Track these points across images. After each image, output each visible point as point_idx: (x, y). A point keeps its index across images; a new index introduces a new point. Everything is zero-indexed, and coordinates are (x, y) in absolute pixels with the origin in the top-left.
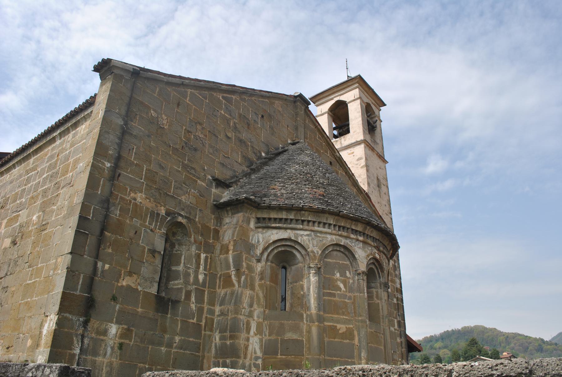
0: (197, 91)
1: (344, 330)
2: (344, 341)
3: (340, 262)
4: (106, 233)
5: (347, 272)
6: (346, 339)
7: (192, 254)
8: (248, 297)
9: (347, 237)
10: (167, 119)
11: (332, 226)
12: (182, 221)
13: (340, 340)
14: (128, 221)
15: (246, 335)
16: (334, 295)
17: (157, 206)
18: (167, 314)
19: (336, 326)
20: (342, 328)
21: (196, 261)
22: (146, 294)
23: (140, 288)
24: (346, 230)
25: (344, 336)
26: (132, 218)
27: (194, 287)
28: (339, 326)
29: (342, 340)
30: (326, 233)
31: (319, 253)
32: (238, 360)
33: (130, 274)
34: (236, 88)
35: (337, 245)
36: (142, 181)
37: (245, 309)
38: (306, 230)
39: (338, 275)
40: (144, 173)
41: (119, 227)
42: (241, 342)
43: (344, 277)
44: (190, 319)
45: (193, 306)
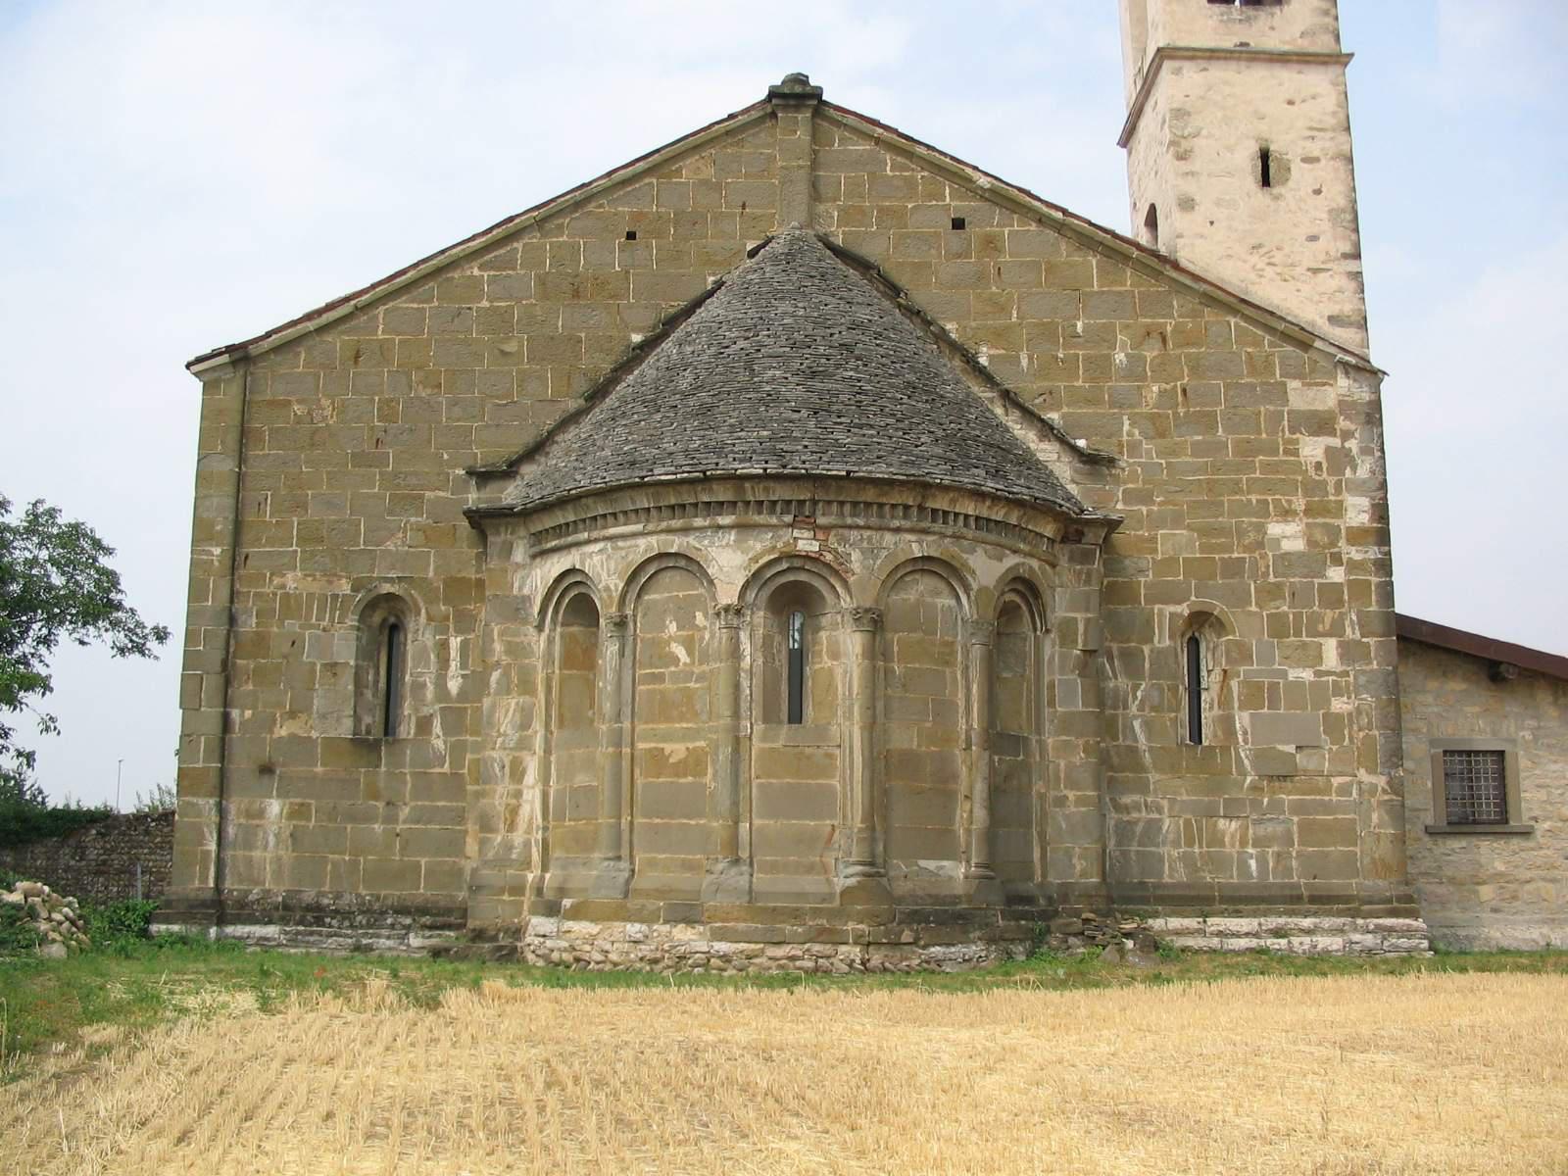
0: (404, 298)
1: (682, 755)
2: (682, 780)
3: (681, 594)
4: (238, 661)
5: (697, 614)
7: (425, 646)
9: (686, 530)
10: (333, 403)
11: (653, 512)
12: (392, 590)
14: (275, 629)
15: (512, 787)
16: (659, 678)
17: (330, 582)
18: (378, 766)
19: (663, 749)
20: (676, 750)
21: (438, 656)
22: (329, 742)
23: (314, 734)
25: (681, 768)
26: (281, 621)
28: (668, 747)
30: (634, 535)
32: (489, 835)
33: (292, 715)
34: (517, 221)
35: (661, 556)
36: (294, 548)
37: (505, 735)
38: (596, 540)
39: (673, 628)
40: (295, 533)
41: (261, 643)
42: (497, 803)
43: (689, 630)
44: (434, 767)
45: (439, 744)
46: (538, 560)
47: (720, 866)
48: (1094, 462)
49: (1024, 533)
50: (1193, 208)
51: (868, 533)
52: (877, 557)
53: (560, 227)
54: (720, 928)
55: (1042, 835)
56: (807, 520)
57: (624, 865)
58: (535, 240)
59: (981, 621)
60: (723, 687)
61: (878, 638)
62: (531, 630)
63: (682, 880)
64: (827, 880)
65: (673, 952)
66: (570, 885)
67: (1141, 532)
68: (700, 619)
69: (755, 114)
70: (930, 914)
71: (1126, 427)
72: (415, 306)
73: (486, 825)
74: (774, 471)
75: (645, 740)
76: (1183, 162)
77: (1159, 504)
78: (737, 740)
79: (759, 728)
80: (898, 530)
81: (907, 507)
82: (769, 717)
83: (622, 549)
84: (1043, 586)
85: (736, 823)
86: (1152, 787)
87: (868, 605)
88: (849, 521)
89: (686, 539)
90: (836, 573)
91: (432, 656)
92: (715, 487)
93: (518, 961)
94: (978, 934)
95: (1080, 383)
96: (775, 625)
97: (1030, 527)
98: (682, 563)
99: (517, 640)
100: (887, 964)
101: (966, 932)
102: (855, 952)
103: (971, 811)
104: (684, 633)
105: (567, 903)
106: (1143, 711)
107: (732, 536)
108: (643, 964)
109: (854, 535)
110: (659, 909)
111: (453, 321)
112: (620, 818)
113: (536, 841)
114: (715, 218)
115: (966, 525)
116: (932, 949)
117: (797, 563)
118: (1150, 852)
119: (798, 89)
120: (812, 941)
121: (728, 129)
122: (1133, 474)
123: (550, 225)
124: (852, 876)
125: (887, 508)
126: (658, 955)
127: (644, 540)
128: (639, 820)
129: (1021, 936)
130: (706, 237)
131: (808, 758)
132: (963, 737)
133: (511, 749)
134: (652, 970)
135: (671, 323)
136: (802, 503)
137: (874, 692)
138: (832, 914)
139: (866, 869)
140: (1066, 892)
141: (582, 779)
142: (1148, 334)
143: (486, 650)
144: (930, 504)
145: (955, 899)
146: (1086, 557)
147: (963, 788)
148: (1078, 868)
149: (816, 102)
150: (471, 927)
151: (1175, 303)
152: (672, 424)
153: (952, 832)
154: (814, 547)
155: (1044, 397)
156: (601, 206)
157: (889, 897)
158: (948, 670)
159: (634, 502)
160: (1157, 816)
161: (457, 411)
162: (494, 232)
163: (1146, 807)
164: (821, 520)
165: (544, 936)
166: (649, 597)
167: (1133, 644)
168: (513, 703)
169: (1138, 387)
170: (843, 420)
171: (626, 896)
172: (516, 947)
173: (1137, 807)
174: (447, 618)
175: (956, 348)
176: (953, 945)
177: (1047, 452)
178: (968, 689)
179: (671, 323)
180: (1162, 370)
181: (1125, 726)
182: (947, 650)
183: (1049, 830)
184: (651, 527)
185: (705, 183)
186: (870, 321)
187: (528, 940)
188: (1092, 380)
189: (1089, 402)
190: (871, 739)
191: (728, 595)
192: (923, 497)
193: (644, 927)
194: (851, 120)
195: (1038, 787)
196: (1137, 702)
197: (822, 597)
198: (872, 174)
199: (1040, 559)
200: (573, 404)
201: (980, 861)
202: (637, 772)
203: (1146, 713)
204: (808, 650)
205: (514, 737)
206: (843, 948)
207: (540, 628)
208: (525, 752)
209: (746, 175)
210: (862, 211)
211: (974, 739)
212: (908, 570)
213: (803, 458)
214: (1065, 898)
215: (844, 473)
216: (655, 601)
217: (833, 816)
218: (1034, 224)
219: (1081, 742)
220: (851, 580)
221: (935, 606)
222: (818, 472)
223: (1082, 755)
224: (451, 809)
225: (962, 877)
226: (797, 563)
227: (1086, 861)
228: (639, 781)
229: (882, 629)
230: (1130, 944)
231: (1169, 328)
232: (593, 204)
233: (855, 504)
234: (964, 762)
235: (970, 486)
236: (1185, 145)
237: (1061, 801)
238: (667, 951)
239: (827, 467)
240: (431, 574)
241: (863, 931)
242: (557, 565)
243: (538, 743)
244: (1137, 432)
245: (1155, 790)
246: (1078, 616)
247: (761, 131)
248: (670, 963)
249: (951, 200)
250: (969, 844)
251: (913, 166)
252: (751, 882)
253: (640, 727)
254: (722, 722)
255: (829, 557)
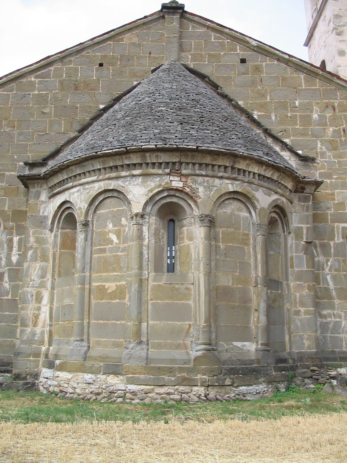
1: (114, 288)
2: (113, 301)
3: (115, 210)
5: (122, 219)
6: (115, 299)
8: (39, 269)
9: (117, 178)
11: (102, 171)
13: (108, 301)
16: (103, 251)
20: (111, 286)
21: (8, 245)
24: (93, 173)
25: (113, 295)
27: (6, 268)
28: (107, 285)
29: (110, 301)
30: (93, 182)
31: (86, 208)
35: (106, 191)
37: (34, 280)
38: (76, 186)
39: (110, 226)
42: (29, 313)
44: (4, 296)
46: (52, 199)
47: (132, 345)
48: (304, 159)
49: (280, 185)
50: (344, 55)
51: (207, 178)
52: (211, 191)
53: (70, 61)
54: (132, 377)
55: (289, 329)
56: (177, 172)
57: (85, 344)
58: (59, 66)
59: (262, 224)
60: (134, 255)
61: (212, 230)
62: (48, 232)
63: (112, 352)
64: (187, 352)
65: (107, 389)
66: (60, 353)
67: (327, 191)
68: (124, 221)
69: (155, 17)
70: (239, 370)
71: (319, 146)
72: (6, 93)
73: (24, 324)
74: (161, 146)
75: (96, 281)
76: (339, 36)
77: (336, 179)
78: (141, 281)
79: (152, 274)
80: (221, 178)
81: (226, 167)
82: (158, 269)
83: (87, 189)
84: (287, 211)
85: (140, 323)
86: (336, 306)
87: (207, 213)
88: (198, 172)
89: (118, 182)
90: (191, 198)
91: (5, 245)
92: (131, 156)
93: (36, 390)
94: (263, 379)
95: (298, 127)
96: (161, 224)
97: (282, 182)
98: (116, 194)
99: (41, 236)
100: (218, 397)
101: (257, 379)
102: (201, 390)
103: (258, 317)
104: (116, 228)
105: (58, 362)
106: (331, 271)
107: (140, 179)
108: (92, 395)
109: (200, 179)
110: (101, 366)
111: (22, 99)
112: (83, 320)
113: (47, 331)
114: (137, 58)
115: (254, 178)
116: (241, 388)
117: (172, 193)
118: (336, 337)
119: (174, 5)
120: (178, 385)
121: (144, 22)
122: (323, 165)
123: (66, 60)
124: (199, 350)
125: (216, 167)
126: (100, 391)
127: (98, 184)
128: (93, 321)
129: (283, 379)
130: (134, 66)
131: (177, 290)
132: (254, 280)
133: (36, 287)
134: (96, 399)
135: (117, 100)
136: (174, 163)
137: (210, 257)
138: (190, 371)
139: (207, 347)
140: (301, 357)
141: (67, 301)
142: (327, 106)
143: (27, 240)
144: (237, 166)
145: (252, 362)
146: (306, 199)
147: (254, 304)
148: (306, 344)
149: (181, 11)
150: (14, 373)
151: (338, 94)
152: (113, 131)
153: (249, 327)
154: (180, 185)
155: (282, 132)
156: (88, 53)
157: (218, 361)
158: (246, 247)
159: (93, 166)
160: (339, 320)
161: (22, 138)
162: (41, 62)
163: (334, 316)
164: (184, 172)
165: (47, 378)
166: (99, 212)
167: (326, 241)
168: (38, 265)
169: (324, 129)
170: (194, 127)
171: (85, 360)
172: (35, 383)
173: (330, 316)
174: (12, 228)
175: (243, 111)
176: (251, 385)
177: (286, 155)
178: (256, 257)
179: (117, 100)
180: (334, 121)
181: (323, 278)
182: (246, 238)
183: (292, 327)
184: (101, 177)
185: (134, 44)
186: (206, 93)
187: (41, 379)
188: (304, 125)
189: (302, 135)
190: (209, 279)
191: (137, 208)
192: (234, 162)
193: (93, 376)
194: (196, 19)
195: (287, 306)
196: (328, 267)
197: (184, 210)
198: (205, 41)
199: (286, 198)
200: (72, 135)
201: (263, 342)
202: (92, 297)
203: (332, 272)
204: (177, 237)
205: (38, 281)
206: (195, 388)
207: (51, 230)
208: (43, 289)
209: (152, 41)
210: (201, 55)
211: (259, 281)
212: (227, 198)
213: (175, 141)
214: (301, 359)
215: (195, 147)
216: (102, 213)
217: (190, 320)
218: (276, 61)
219: (306, 284)
220: (199, 201)
221: (240, 217)
222: (182, 146)
223: (307, 291)
224: (11, 316)
225: (254, 350)
226: (172, 193)
227: (310, 342)
228: (93, 302)
229: (214, 226)
230: (335, 382)
231: (336, 104)
232: (85, 52)
233: (201, 165)
234: (254, 292)
235: (256, 157)
236: (340, 29)
237: (297, 313)
238: (104, 389)
239: (187, 144)
240: (6, 209)
241: (205, 379)
242: (59, 200)
243: (49, 285)
244: (324, 147)
245: (338, 308)
246: (304, 226)
247: (158, 24)
248: (105, 396)
249: (240, 51)
250: (257, 333)
251: (223, 38)
252: (147, 353)
253: (94, 275)
254: (133, 271)
255: (188, 190)
